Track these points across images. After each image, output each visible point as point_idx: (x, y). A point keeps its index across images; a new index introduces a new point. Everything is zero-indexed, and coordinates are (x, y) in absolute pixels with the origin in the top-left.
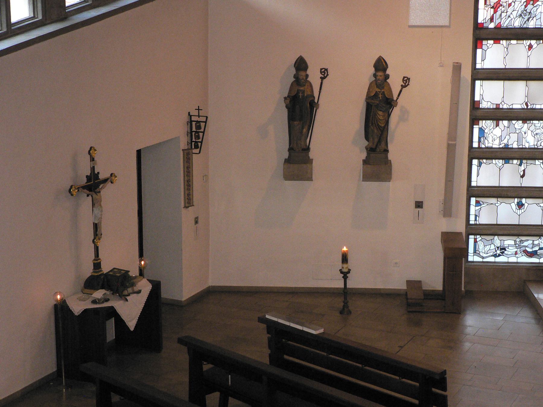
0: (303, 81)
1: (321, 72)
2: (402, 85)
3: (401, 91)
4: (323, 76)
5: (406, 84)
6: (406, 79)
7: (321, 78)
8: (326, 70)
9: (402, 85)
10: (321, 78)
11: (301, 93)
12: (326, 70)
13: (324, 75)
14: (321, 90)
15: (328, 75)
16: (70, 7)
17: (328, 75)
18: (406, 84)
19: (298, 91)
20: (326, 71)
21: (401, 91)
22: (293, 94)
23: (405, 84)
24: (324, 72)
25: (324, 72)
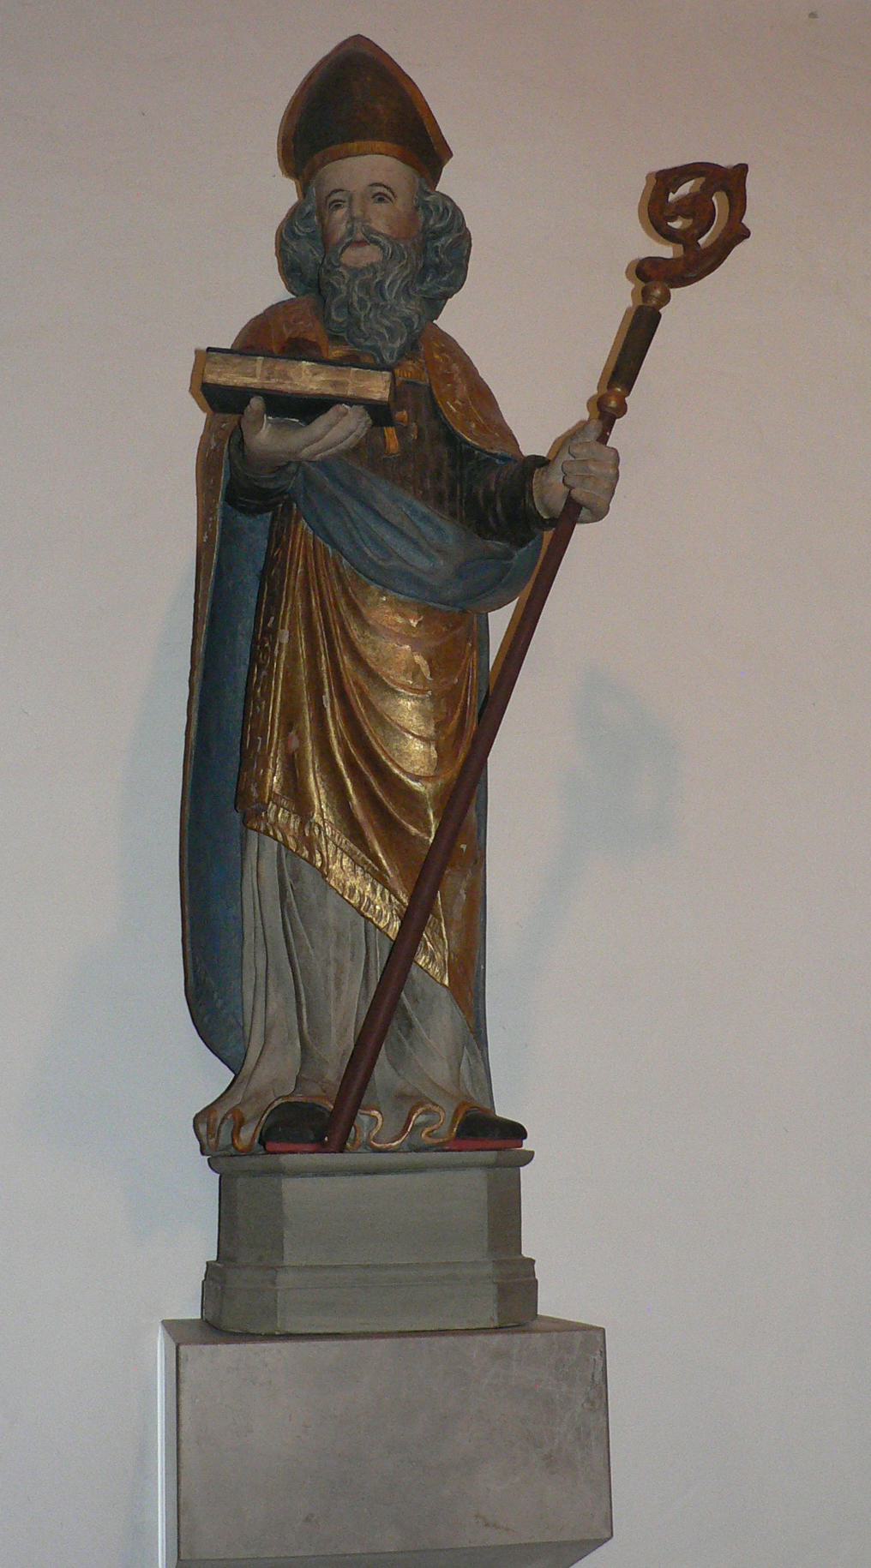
4: (666, 251)
17: (746, 234)
24: (697, 207)
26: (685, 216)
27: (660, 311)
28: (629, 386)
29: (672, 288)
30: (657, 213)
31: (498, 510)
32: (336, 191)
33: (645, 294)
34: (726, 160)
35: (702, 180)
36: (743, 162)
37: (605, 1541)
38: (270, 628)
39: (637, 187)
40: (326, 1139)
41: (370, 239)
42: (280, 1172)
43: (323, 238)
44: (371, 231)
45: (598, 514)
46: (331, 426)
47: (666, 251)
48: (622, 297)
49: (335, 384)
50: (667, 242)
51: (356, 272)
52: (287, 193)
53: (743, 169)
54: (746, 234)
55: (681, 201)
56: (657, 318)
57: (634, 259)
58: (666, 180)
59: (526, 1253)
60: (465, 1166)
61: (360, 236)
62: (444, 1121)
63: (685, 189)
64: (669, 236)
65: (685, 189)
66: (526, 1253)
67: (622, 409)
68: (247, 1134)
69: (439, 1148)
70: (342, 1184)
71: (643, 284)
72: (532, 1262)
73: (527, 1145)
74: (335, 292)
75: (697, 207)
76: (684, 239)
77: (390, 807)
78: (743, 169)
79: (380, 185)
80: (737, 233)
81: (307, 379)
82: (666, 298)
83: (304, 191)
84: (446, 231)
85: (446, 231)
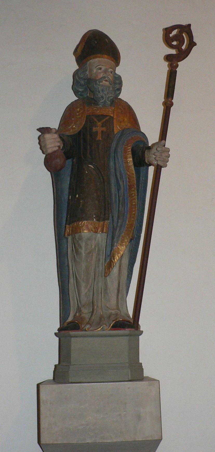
4: (173, 52)
17: (195, 44)
22: (74, 128)
24: (179, 38)
26: (176, 41)
27: (177, 70)
29: (179, 62)
30: (168, 41)
31: (146, 162)
34: (184, 23)
35: (179, 29)
36: (190, 23)
38: (70, 196)
40: (77, 196)
42: (71, 337)
47: (173, 52)
48: (165, 67)
50: (169, 47)
53: (189, 25)
54: (195, 44)
56: (176, 72)
57: (166, 54)
58: (167, 31)
59: (140, 362)
63: (175, 32)
64: (172, 47)
65: (175, 32)
66: (141, 330)
67: (172, 104)
71: (170, 63)
72: (141, 363)
75: (179, 38)
76: (177, 48)
80: (192, 44)
82: (177, 66)
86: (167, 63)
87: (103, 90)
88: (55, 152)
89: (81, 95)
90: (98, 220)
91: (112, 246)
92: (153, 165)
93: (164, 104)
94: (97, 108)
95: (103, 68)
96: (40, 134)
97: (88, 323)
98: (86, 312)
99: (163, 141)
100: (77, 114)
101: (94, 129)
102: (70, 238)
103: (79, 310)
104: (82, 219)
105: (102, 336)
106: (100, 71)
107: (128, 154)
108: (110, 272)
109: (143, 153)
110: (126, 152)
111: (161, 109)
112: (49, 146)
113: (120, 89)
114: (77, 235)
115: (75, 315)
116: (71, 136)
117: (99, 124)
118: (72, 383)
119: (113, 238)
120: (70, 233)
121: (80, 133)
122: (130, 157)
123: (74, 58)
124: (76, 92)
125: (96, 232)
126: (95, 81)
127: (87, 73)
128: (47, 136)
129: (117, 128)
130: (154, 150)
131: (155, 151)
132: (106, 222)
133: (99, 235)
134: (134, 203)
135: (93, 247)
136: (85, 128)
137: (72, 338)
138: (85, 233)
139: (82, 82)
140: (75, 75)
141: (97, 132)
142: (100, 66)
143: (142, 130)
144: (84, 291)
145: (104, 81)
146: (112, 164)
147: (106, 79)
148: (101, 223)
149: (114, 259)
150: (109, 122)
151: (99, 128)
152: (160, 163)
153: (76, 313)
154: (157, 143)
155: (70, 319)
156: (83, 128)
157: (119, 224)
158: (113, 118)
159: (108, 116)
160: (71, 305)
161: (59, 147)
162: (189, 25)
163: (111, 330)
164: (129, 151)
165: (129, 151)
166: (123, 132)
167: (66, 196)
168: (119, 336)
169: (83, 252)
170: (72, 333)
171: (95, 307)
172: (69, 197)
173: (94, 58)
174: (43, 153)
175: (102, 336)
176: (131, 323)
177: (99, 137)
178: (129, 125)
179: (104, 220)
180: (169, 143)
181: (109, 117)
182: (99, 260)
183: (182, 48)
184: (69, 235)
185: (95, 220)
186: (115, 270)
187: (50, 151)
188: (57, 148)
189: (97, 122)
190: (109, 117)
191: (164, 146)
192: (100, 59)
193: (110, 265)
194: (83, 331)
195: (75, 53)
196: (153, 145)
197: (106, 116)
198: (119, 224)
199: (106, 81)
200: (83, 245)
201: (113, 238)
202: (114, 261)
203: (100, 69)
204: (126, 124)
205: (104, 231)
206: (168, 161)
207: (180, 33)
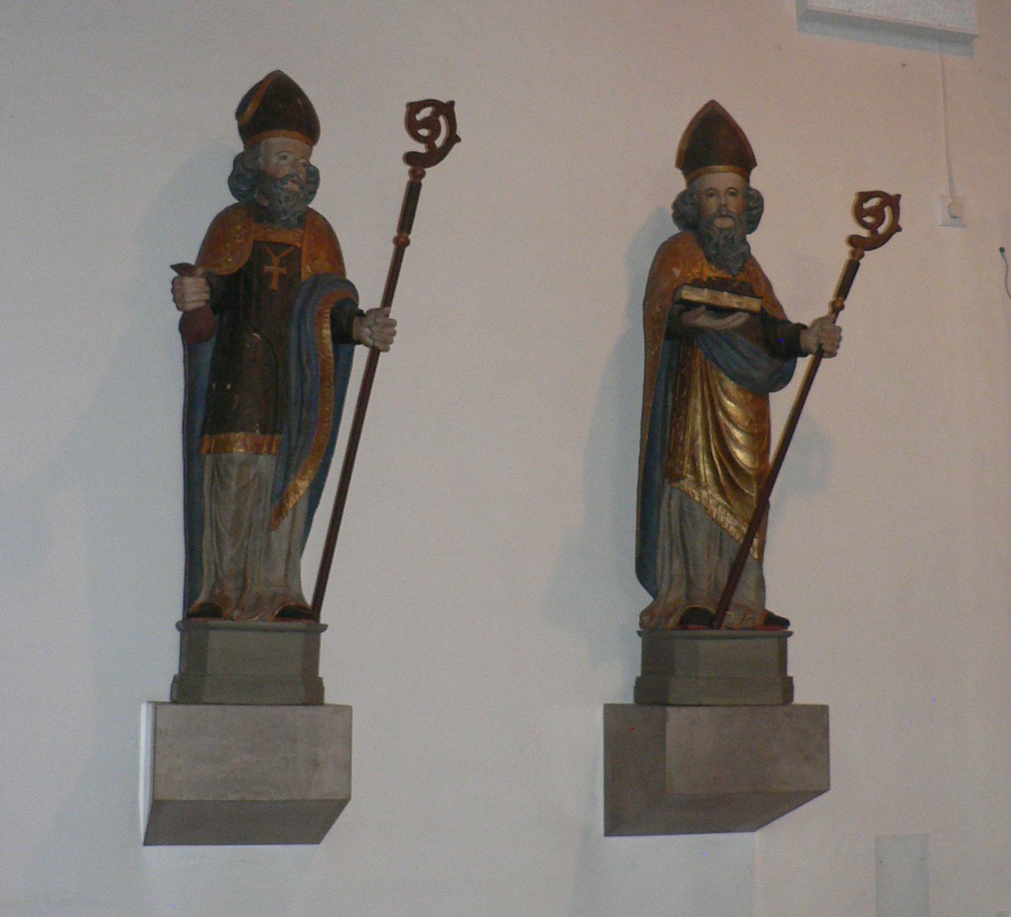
0: (296, 188)
1: (859, 213)
2: (854, 241)
3: (851, 270)
4: (864, 233)
5: (439, 142)
6: (426, 112)
7: (410, 158)
8: (446, 109)
9: (854, 241)
10: (410, 158)
11: (275, 259)
12: (446, 109)
13: (428, 141)
14: (409, 230)
15: (899, 229)
16: (709, 413)
17: (458, 140)
18: (439, 142)
19: (260, 252)
20: (442, 119)
21: (851, 270)
22: (230, 264)
23: (872, 228)
24: (431, 124)
25: (431, 124)
28: (845, 298)
30: (412, 126)
32: (711, 189)
33: (853, 253)
34: (892, 192)
37: (825, 791)
39: (852, 199)
40: (229, 386)
41: (728, 216)
43: (700, 208)
44: (728, 211)
45: (832, 354)
46: (735, 320)
48: (403, 173)
49: (739, 303)
51: (722, 230)
52: (679, 183)
54: (458, 140)
55: (871, 208)
56: (858, 265)
58: (864, 197)
60: (770, 637)
61: (724, 213)
62: (759, 621)
66: (323, 621)
68: (673, 621)
69: (753, 629)
70: (723, 644)
73: (790, 629)
74: (711, 239)
77: (737, 480)
78: (899, 197)
79: (732, 188)
80: (895, 228)
81: (726, 299)
82: (423, 175)
83: (690, 182)
84: (756, 208)
85: (756, 208)
86: (408, 168)
87: (287, 199)
88: (198, 310)
89: (243, 197)
90: (263, 432)
91: (286, 478)
92: (366, 345)
93: (396, 241)
94: (273, 228)
95: (291, 157)
96: (175, 274)
97: (237, 607)
98: (231, 588)
99: (387, 309)
100: (237, 236)
101: (267, 268)
102: (208, 459)
103: (218, 582)
104: (231, 429)
105: (259, 629)
106: (284, 162)
107: (325, 322)
108: (279, 523)
109: (350, 322)
110: (321, 313)
111: (391, 248)
112: (188, 299)
113: (313, 193)
114: (224, 456)
115: (211, 593)
116: (219, 277)
117: (275, 259)
118: (207, 704)
119: (288, 467)
120: (212, 450)
121: (238, 274)
122: (326, 328)
123: (234, 124)
124: (234, 191)
125: (258, 453)
126: (274, 180)
127: (260, 160)
128: (188, 280)
129: (307, 271)
130: (370, 321)
131: (372, 322)
132: (277, 437)
133: (261, 458)
134: (327, 409)
135: (251, 476)
136: (249, 264)
137: (212, 633)
138: (239, 451)
139: (249, 176)
140: (238, 160)
141: (270, 274)
142: (285, 154)
143: (350, 276)
144: (229, 552)
145: (290, 183)
146: (293, 335)
147: (295, 178)
148: (268, 437)
149: (288, 502)
150: (292, 258)
151: (274, 268)
152: (377, 344)
153: (214, 588)
154: (377, 310)
155: (202, 598)
156: (246, 265)
157: (300, 443)
158: (300, 249)
159: (291, 245)
160: (205, 574)
161: (206, 301)
162: (452, 103)
163: (274, 621)
164: (326, 318)
165: (326, 318)
166: (317, 278)
167: (204, 381)
168: (283, 631)
169: (233, 485)
170: (212, 622)
171: (249, 581)
172: (210, 385)
173: (275, 136)
174: (179, 309)
175: (259, 629)
176: (308, 610)
177: (274, 285)
178: (327, 265)
179: (275, 431)
180: (395, 312)
181: (293, 248)
182: (260, 501)
183: (434, 144)
184: (208, 452)
185: (258, 432)
186: (287, 520)
187: (190, 307)
188: (203, 304)
189: (273, 255)
190: (293, 248)
191: (388, 316)
192: (287, 140)
193: (280, 512)
194: (226, 619)
195: (240, 113)
196: (371, 311)
197: (288, 246)
198: (300, 443)
199: (294, 182)
200: (234, 472)
201: (288, 467)
202: (287, 506)
203: (285, 158)
204: (324, 266)
205: (274, 450)
206: (391, 342)
207: (435, 114)
